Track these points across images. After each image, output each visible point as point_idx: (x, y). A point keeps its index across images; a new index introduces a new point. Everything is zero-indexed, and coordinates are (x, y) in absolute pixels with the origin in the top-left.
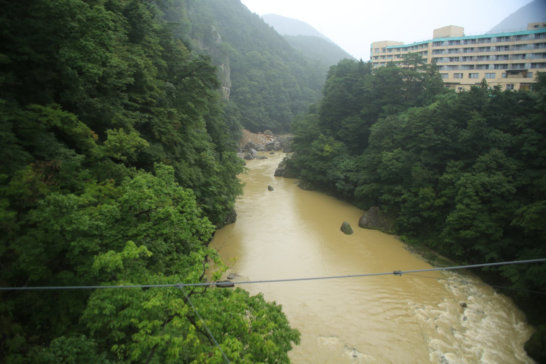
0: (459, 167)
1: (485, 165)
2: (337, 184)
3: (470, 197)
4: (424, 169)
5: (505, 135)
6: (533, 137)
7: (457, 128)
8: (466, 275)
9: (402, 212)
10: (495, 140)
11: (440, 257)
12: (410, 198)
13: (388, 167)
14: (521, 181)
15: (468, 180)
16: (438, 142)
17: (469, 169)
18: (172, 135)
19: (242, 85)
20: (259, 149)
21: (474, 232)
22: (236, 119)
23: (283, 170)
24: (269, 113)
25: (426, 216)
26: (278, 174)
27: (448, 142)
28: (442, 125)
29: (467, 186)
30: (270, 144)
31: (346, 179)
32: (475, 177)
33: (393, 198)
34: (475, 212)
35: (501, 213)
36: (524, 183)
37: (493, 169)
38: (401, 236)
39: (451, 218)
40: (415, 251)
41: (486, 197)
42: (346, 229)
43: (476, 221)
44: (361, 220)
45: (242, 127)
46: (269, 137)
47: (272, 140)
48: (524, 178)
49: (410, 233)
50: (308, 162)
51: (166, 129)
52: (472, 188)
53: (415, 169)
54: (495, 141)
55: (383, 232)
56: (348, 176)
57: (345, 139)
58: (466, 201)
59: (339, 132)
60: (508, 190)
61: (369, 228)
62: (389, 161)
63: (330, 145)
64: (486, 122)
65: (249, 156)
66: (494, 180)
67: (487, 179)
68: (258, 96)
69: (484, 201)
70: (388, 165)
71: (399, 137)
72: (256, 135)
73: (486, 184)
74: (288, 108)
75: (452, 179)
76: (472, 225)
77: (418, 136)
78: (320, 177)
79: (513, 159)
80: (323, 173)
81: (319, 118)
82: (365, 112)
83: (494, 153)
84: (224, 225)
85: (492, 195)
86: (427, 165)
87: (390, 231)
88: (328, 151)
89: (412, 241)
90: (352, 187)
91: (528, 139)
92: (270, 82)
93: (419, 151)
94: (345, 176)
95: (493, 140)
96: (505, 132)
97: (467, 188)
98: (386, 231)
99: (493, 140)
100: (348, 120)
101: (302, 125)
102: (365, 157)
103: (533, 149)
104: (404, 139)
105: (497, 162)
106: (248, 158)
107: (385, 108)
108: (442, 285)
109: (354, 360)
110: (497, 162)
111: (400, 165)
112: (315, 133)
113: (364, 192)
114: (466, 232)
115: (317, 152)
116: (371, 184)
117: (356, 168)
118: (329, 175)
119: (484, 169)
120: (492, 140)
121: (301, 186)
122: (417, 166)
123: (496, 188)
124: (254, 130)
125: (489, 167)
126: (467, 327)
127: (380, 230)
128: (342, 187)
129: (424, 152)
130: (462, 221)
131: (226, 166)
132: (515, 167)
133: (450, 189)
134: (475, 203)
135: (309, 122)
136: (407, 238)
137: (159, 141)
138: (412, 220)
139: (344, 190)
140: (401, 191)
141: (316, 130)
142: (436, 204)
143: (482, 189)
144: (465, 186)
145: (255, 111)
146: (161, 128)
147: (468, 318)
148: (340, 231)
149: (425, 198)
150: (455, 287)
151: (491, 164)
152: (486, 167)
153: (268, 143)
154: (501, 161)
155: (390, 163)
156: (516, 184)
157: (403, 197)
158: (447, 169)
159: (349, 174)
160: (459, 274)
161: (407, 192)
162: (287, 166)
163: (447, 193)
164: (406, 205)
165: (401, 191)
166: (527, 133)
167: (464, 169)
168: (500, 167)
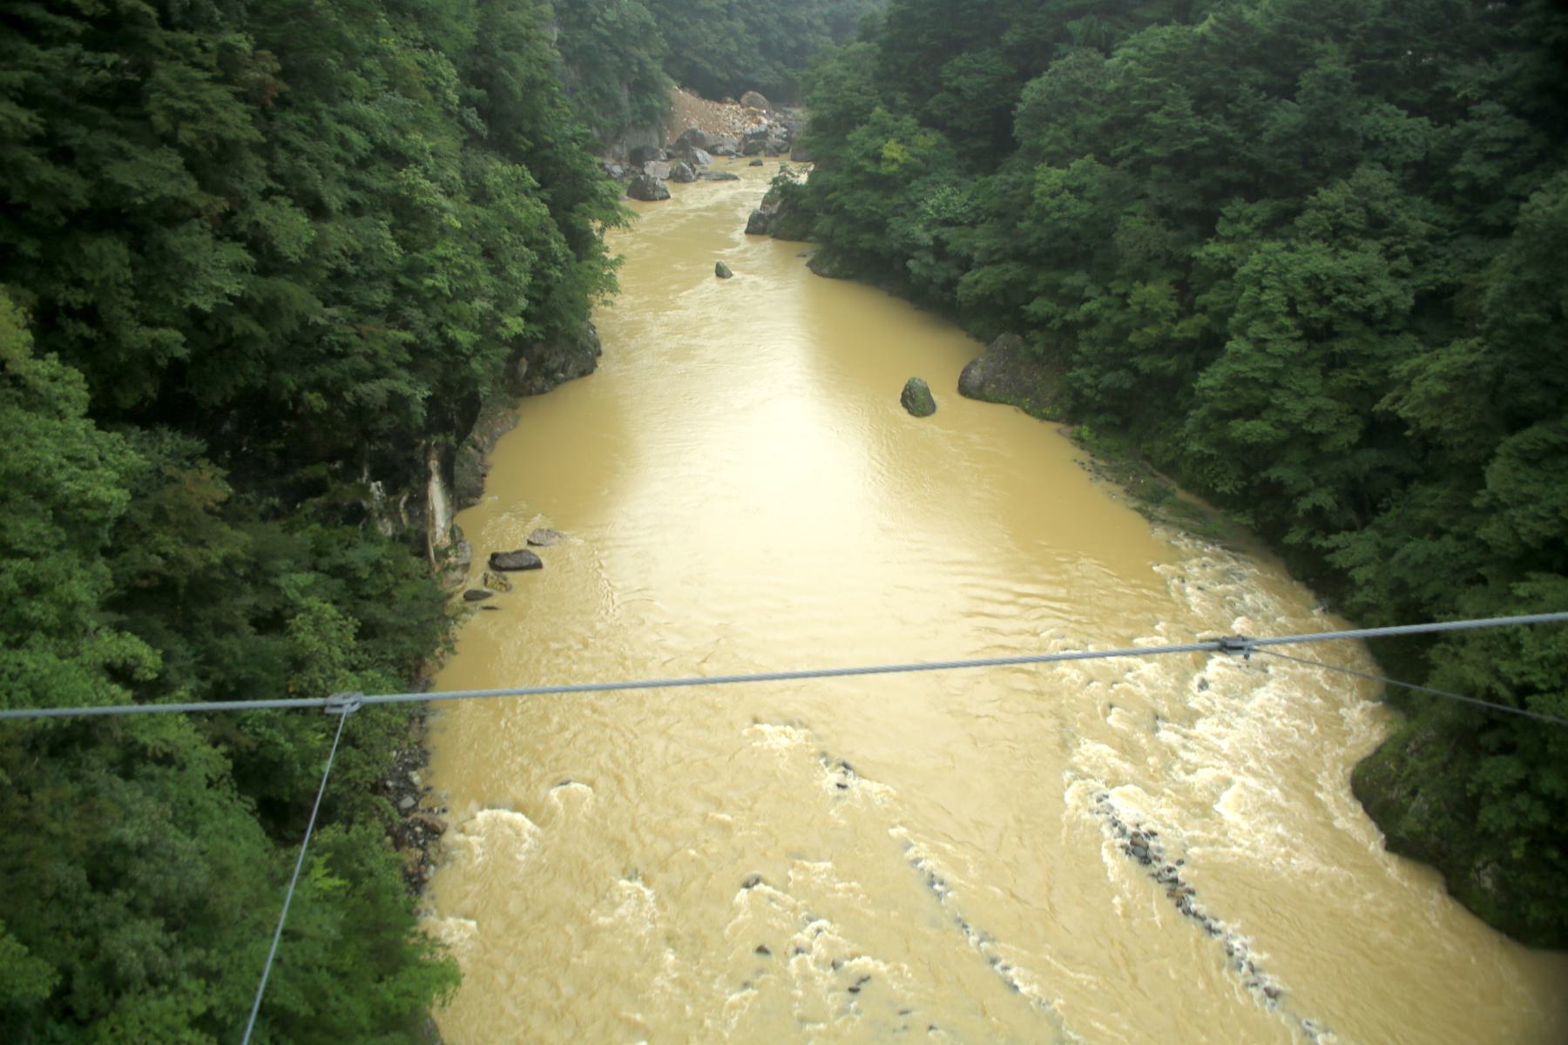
0: (1256, 220)
1: (1329, 219)
2: (911, 263)
3: (1269, 317)
4: (1152, 223)
5: (1411, 121)
6: (1492, 131)
7: (1264, 95)
8: (1243, 552)
9: (1080, 353)
10: (1377, 137)
11: (1182, 495)
12: (1107, 313)
13: (1047, 214)
14: (1436, 272)
15: (1269, 263)
17: (1285, 230)
18: (221, 122)
20: (720, 150)
21: (1272, 425)
22: (650, 57)
23: (771, 216)
24: (758, 40)
26: (757, 227)
27: (1231, 140)
28: (1220, 87)
29: (1265, 282)
30: (755, 135)
31: (940, 249)
32: (1292, 256)
33: (1060, 310)
34: (1280, 364)
35: (1361, 371)
36: (1445, 278)
37: (1352, 230)
38: (1077, 428)
39: (1209, 380)
40: (1108, 475)
41: (1316, 319)
42: (916, 401)
43: (1279, 393)
44: (966, 371)
45: (669, 80)
46: (754, 114)
47: (765, 121)
48: (1448, 263)
49: (1101, 419)
50: (837, 194)
51: (198, 102)
52: (1279, 290)
53: (1128, 224)
54: (1376, 143)
55: (1027, 412)
56: (944, 237)
57: (949, 124)
58: (1258, 328)
59: (931, 102)
60: (1387, 302)
62: (1053, 196)
63: (902, 141)
64: (1354, 78)
65: (683, 170)
66: (1347, 268)
67: (1328, 263)
69: (1316, 334)
70: (1048, 208)
71: (1091, 122)
72: (717, 105)
73: (1321, 281)
74: (819, 22)
75: (1230, 258)
76: (1267, 405)
77: (1144, 121)
78: (867, 240)
79: (1427, 203)
80: (878, 226)
81: (879, 58)
82: (1016, 38)
83: (1362, 181)
84: (558, 382)
85: (1335, 314)
86: (1164, 211)
87: (1047, 411)
88: (894, 161)
89: (1107, 442)
90: (954, 272)
91: (1478, 137)
93: (1140, 168)
94: (936, 239)
95: (1371, 137)
96: (1414, 111)
97: (1262, 289)
98: (1036, 411)
99: (1371, 137)
100: (962, 64)
101: (828, 80)
102: (999, 180)
103: (1488, 171)
104: (1108, 129)
105: (1369, 211)
106: (679, 177)
107: (1075, 26)
108: (1163, 581)
110: (1369, 211)
111: (1084, 209)
112: (860, 103)
113: (978, 290)
114: (1248, 425)
115: (860, 163)
116: (1004, 266)
117: (973, 215)
118: (893, 235)
119: (1326, 230)
120: (1365, 137)
121: (816, 267)
122: (1133, 214)
123: (1351, 293)
124: (713, 91)
125: (1343, 226)
126: (1202, 710)
127: (1018, 405)
128: (924, 273)
129: (1155, 169)
130: (1237, 390)
131: (499, 209)
132: (1423, 228)
133: (1223, 289)
134: (1283, 336)
135: (848, 69)
136: (1094, 434)
137: (169, 140)
138: (1109, 379)
139: (930, 281)
140: (1082, 289)
141: (865, 94)
142: (1175, 335)
143: (1307, 294)
144: (1258, 283)
145: (715, 31)
146: (178, 98)
147: (1211, 685)
148: (900, 405)
149: (1147, 316)
150: (1200, 588)
151: (1348, 216)
152: (1332, 224)
153: (748, 131)
154: (1381, 207)
155: (1055, 202)
156: (1419, 282)
157: (1085, 307)
158: (1218, 228)
159: (946, 233)
160: (1223, 548)
161: (1101, 294)
162: (783, 203)
164: (1094, 333)
165: (1082, 289)
166: (1481, 118)
167: (1269, 229)
168: (1377, 225)
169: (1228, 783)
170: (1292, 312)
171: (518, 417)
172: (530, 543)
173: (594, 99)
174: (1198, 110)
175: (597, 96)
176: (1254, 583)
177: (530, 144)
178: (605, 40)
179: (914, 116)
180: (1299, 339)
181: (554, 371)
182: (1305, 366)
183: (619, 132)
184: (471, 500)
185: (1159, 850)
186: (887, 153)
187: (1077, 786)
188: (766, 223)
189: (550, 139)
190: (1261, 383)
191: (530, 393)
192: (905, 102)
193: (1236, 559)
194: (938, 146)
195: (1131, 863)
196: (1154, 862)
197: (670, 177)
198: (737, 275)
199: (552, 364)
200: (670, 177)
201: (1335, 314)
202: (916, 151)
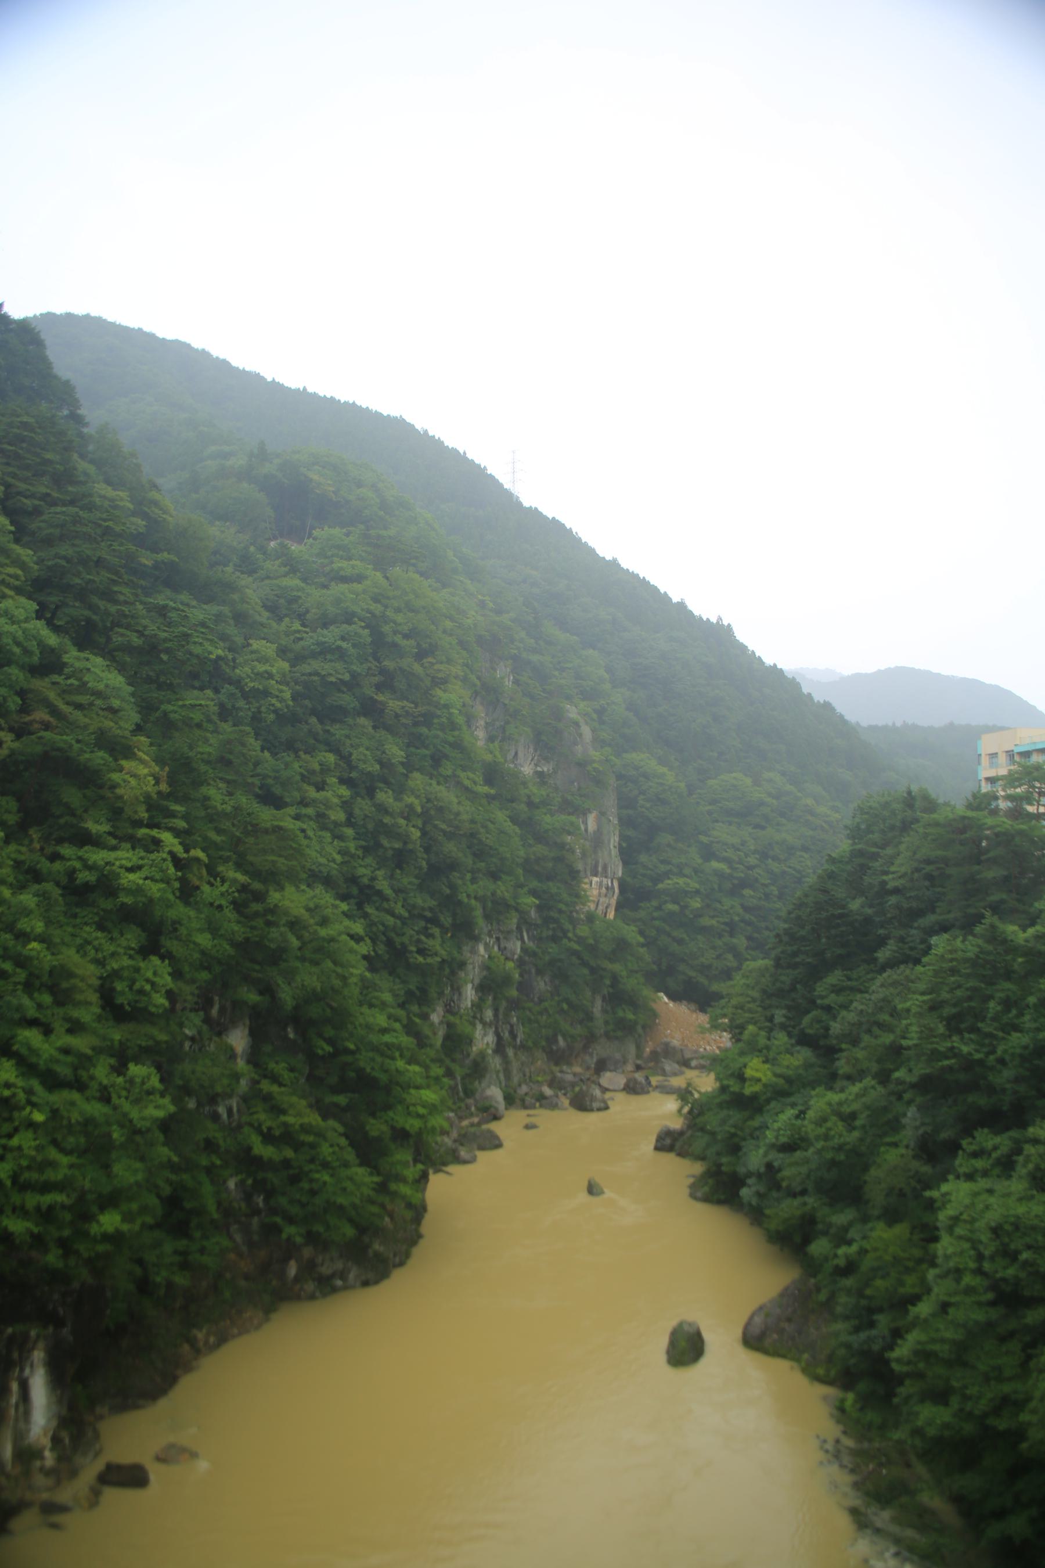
16: (946, 1063)
19: (675, 870)
25: (374, 1133)
40: (846, 1460)
59: (806, 1020)
61: (766, 1352)
65: (635, 1081)
68: (728, 903)
84: (334, 1290)
87: (821, 1371)
88: (759, 1080)
92: (770, 861)
106: (632, 1089)
122: (895, 1145)
141: (750, 1011)
155: (821, 1131)
170: (979, 1272)
173: (562, 1010)
175: (565, 1006)
177: (329, 1049)
178: (575, 953)
179: (790, 1035)
182: (1003, 1339)
183: (591, 1039)
186: (749, 1073)
189: (352, 1047)
192: (783, 1020)
194: (807, 1066)
197: (624, 1089)
198: (608, 1194)
199: (326, 1270)
200: (624, 1089)
201: (1023, 1275)
202: (778, 1070)
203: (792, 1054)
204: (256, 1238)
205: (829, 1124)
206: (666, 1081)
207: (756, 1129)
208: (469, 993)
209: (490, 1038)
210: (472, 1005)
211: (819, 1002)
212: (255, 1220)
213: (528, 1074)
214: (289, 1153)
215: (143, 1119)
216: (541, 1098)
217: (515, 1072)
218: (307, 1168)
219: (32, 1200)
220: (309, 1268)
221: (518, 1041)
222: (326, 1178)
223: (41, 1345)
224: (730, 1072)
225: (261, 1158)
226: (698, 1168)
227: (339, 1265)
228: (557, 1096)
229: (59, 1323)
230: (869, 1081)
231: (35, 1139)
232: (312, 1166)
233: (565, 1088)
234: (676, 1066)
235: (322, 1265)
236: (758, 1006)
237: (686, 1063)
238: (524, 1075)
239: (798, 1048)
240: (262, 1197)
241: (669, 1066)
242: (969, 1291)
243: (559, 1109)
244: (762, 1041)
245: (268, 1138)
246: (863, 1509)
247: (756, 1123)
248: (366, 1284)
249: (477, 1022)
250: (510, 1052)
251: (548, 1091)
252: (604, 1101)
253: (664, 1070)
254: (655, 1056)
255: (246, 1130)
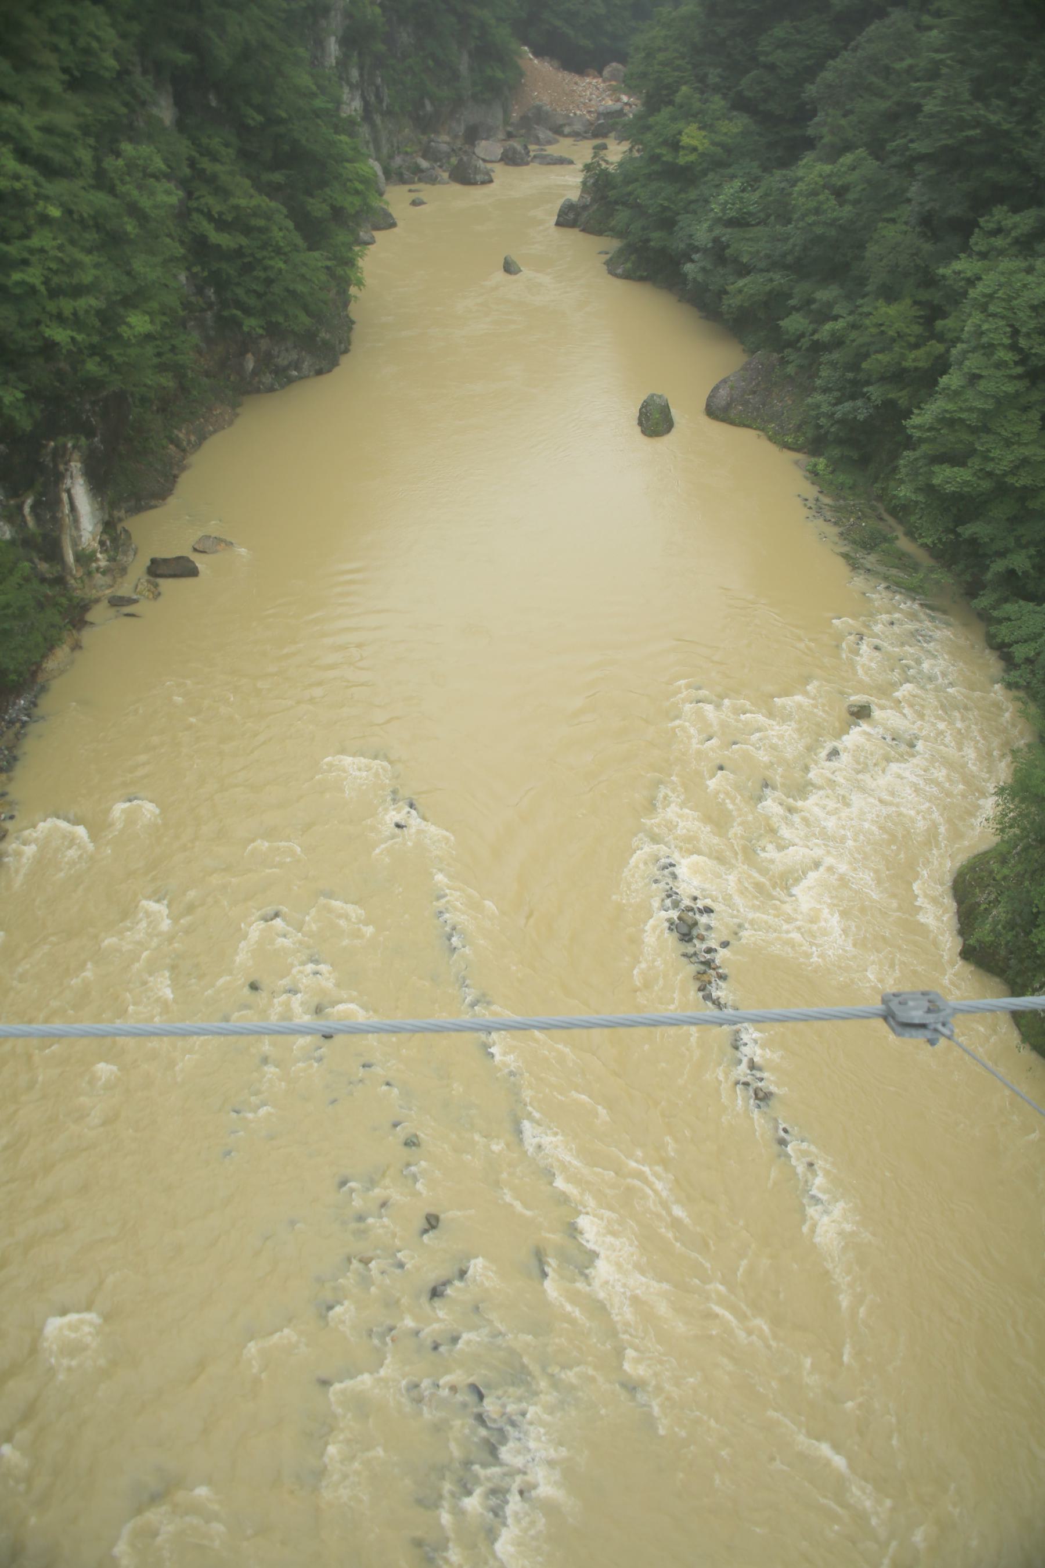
11: (904, 543)
16: (971, 133)
21: (974, 474)
38: (814, 460)
40: (829, 514)
43: (985, 438)
44: (715, 390)
52: (1003, 317)
55: (770, 439)
61: (732, 423)
65: (515, 151)
72: (577, 78)
78: (657, 238)
84: (291, 381)
87: (789, 439)
88: (695, 149)
89: (841, 478)
98: (778, 439)
106: (511, 159)
109: (393, 837)
111: (847, 212)
115: (658, 151)
122: (893, 221)
127: (763, 430)
128: (700, 278)
148: (676, 425)
150: (877, 648)
155: (812, 204)
163: (949, 330)
169: (817, 865)
170: (1014, 347)
171: (237, 415)
172: (195, 550)
174: (978, 95)
175: (431, 63)
176: (938, 647)
177: (260, 118)
179: (725, 96)
180: (1019, 377)
181: (286, 369)
182: (1026, 409)
184: (153, 503)
185: (709, 928)
186: (685, 140)
187: (649, 848)
188: (578, 215)
189: (284, 115)
190: (969, 426)
191: (258, 391)
192: (718, 80)
193: (932, 619)
195: (671, 939)
196: (695, 941)
197: (501, 160)
199: (282, 361)
200: (501, 160)
203: (730, 120)
204: (212, 333)
205: (821, 197)
206: (542, 150)
207: (691, 202)
208: (333, 48)
209: (357, 104)
210: (337, 63)
211: (762, 59)
212: (209, 314)
213: (395, 145)
214: (244, 241)
215: (156, 207)
216: (417, 170)
217: (384, 142)
218: (259, 255)
219: (67, 306)
220: (266, 361)
221: (384, 105)
222: (281, 265)
223: (76, 455)
224: (660, 140)
225: (219, 246)
226: (613, 244)
227: (294, 356)
228: (433, 168)
229: (90, 434)
230: (861, 152)
231: (54, 239)
232: (265, 253)
233: (440, 160)
234: (550, 134)
235: (278, 357)
236: (688, 63)
237: (558, 131)
238: (392, 146)
239: (735, 113)
240: (212, 291)
241: (543, 134)
242: (1000, 365)
243: (440, 183)
244: (697, 105)
245: (221, 225)
246: (852, 555)
247: (693, 194)
248: (319, 372)
249: (344, 83)
250: (378, 119)
251: (424, 164)
252: (487, 173)
253: (538, 138)
254: (526, 122)
255: (195, 216)
